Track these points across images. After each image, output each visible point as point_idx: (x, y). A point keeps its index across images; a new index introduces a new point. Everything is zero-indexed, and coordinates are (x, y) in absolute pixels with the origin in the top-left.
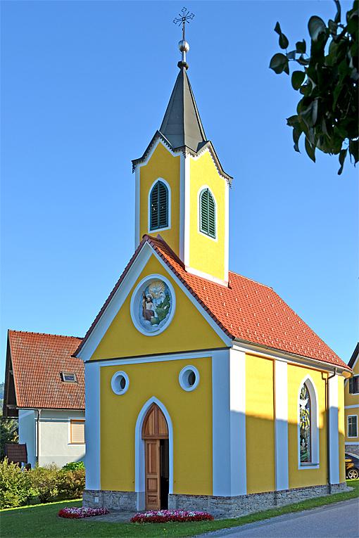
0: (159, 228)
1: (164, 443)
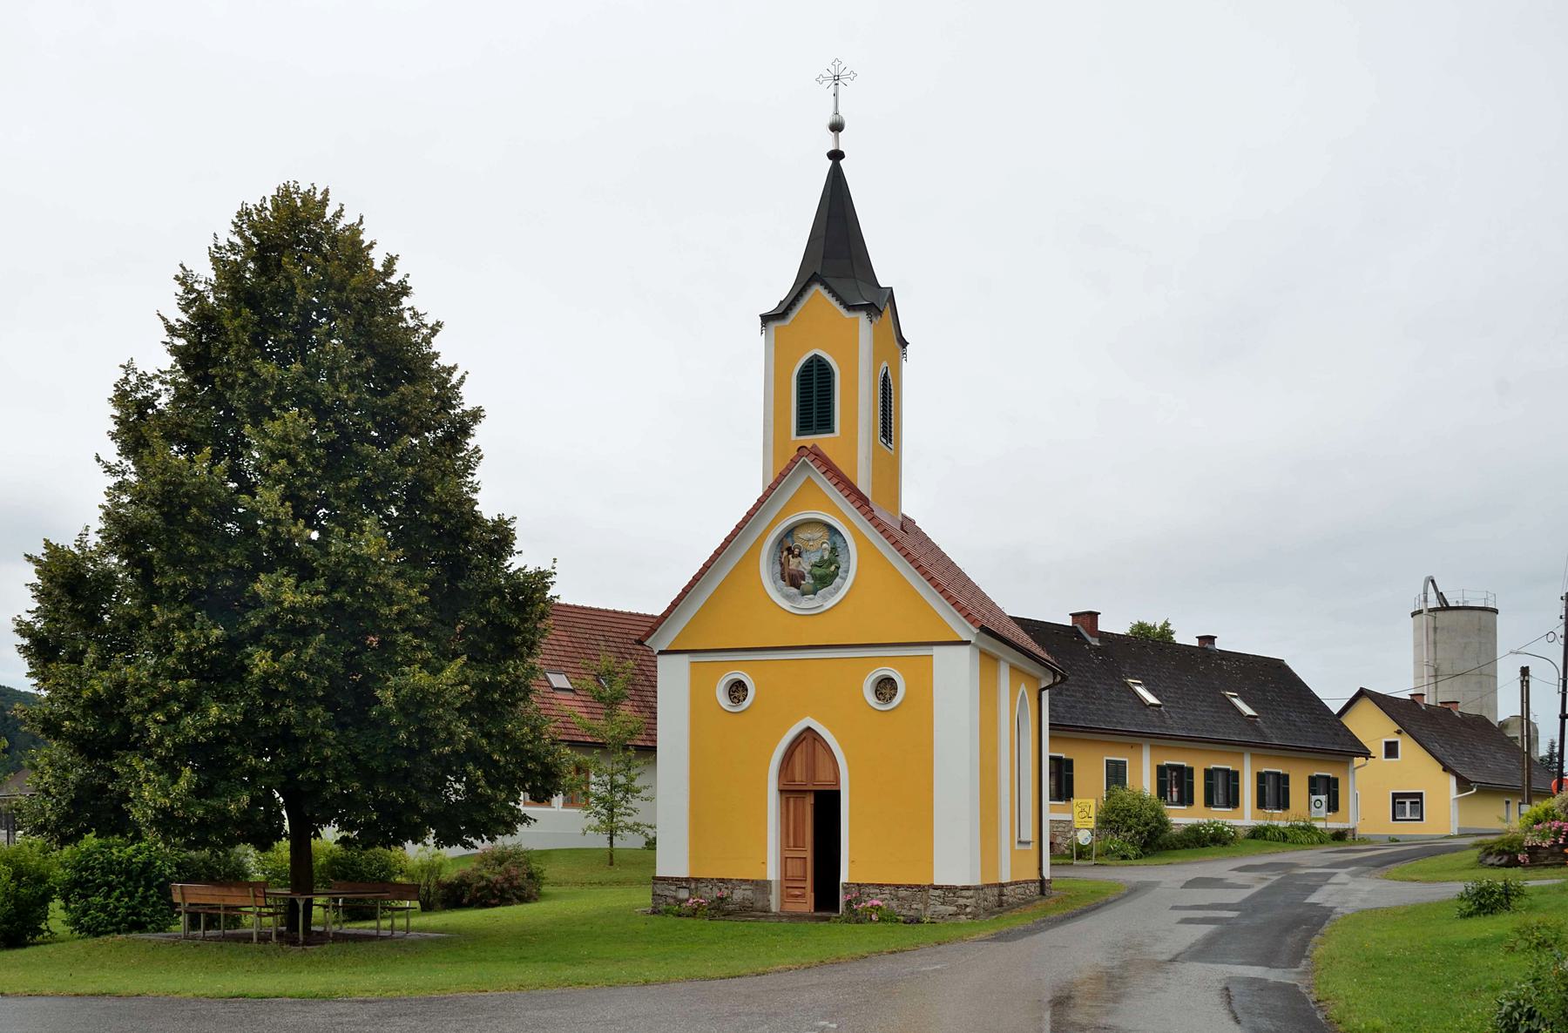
0: (815, 433)
1: (827, 806)
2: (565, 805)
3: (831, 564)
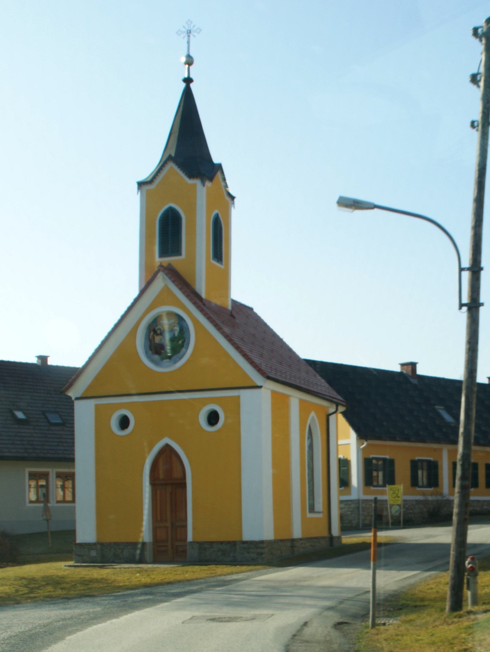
2: (50, 503)
3: (179, 340)
